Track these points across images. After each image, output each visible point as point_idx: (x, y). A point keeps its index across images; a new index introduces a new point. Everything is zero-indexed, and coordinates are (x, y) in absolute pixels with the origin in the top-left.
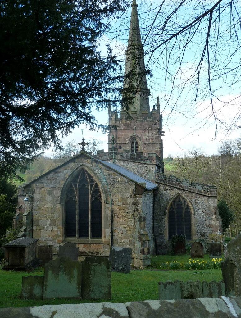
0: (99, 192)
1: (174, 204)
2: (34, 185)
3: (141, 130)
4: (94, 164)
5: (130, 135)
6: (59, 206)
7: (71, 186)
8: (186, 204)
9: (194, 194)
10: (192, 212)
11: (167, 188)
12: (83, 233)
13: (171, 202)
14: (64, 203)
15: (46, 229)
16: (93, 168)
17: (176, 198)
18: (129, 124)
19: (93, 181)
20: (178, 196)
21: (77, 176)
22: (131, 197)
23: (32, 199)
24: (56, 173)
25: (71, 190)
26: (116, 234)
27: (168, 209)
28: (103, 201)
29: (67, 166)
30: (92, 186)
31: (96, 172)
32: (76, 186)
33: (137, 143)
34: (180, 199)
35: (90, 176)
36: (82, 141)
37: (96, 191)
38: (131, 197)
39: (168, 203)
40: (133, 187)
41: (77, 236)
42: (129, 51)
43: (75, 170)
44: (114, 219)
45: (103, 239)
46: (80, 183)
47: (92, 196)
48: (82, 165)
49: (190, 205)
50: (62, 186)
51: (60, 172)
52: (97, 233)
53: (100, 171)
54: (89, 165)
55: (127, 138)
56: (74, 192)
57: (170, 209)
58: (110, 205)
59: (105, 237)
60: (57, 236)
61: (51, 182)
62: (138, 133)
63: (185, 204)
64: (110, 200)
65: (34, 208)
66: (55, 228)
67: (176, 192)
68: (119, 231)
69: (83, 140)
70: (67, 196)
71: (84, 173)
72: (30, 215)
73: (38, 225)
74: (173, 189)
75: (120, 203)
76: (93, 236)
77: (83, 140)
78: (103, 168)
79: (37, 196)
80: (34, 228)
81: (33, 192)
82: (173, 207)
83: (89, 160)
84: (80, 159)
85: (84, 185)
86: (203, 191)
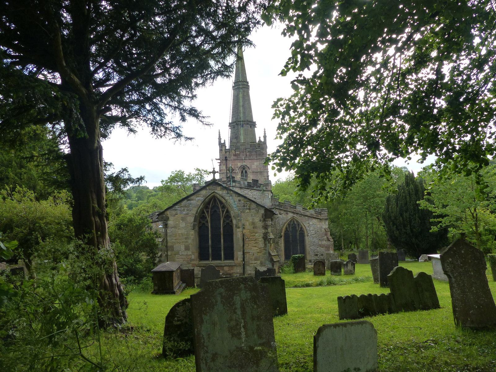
0: (230, 217)
1: (289, 227)
2: (168, 212)
3: (250, 159)
4: (225, 192)
5: (239, 164)
6: (192, 232)
7: (203, 212)
8: (300, 226)
9: (306, 218)
10: (306, 234)
11: (282, 212)
12: (217, 257)
13: (286, 225)
14: (197, 228)
15: (181, 254)
16: (223, 195)
17: (291, 221)
18: (239, 155)
19: (224, 207)
20: (293, 219)
21: (209, 203)
22: (260, 221)
23: (166, 226)
24: (189, 200)
25: (203, 216)
26: (247, 256)
27: (283, 231)
28: (234, 226)
29: (199, 193)
30: (223, 211)
31: (227, 198)
32: (208, 212)
33: (246, 172)
34: (294, 222)
35: (221, 203)
36: (213, 170)
37: (228, 216)
38: (260, 221)
39: (283, 227)
40: (262, 211)
41: (210, 259)
42: (236, 87)
43: (207, 197)
44: (245, 242)
45: (236, 261)
46: (212, 209)
47: (224, 221)
48: (214, 192)
49: (304, 227)
50: (194, 212)
51: (192, 200)
52: (230, 255)
53: (231, 198)
54: (220, 192)
55: (237, 168)
56: (206, 218)
57: (285, 231)
58: (241, 229)
59: (237, 259)
60: (192, 260)
61: (184, 209)
62: (247, 163)
63: (299, 227)
64: (240, 225)
65: (168, 234)
66: (189, 253)
67: (290, 215)
68: (250, 253)
69: (214, 169)
70: (200, 222)
71: (215, 201)
72: (165, 241)
73: (173, 250)
74: (287, 214)
75: (251, 227)
76: (226, 259)
77: (214, 169)
78: (234, 195)
79: (170, 223)
80: (169, 253)
81: (167, 219)
82: (288, 229)
83: (219, 188)
84: (211, 187)
85: (215, 211)
86: (315, 214)
